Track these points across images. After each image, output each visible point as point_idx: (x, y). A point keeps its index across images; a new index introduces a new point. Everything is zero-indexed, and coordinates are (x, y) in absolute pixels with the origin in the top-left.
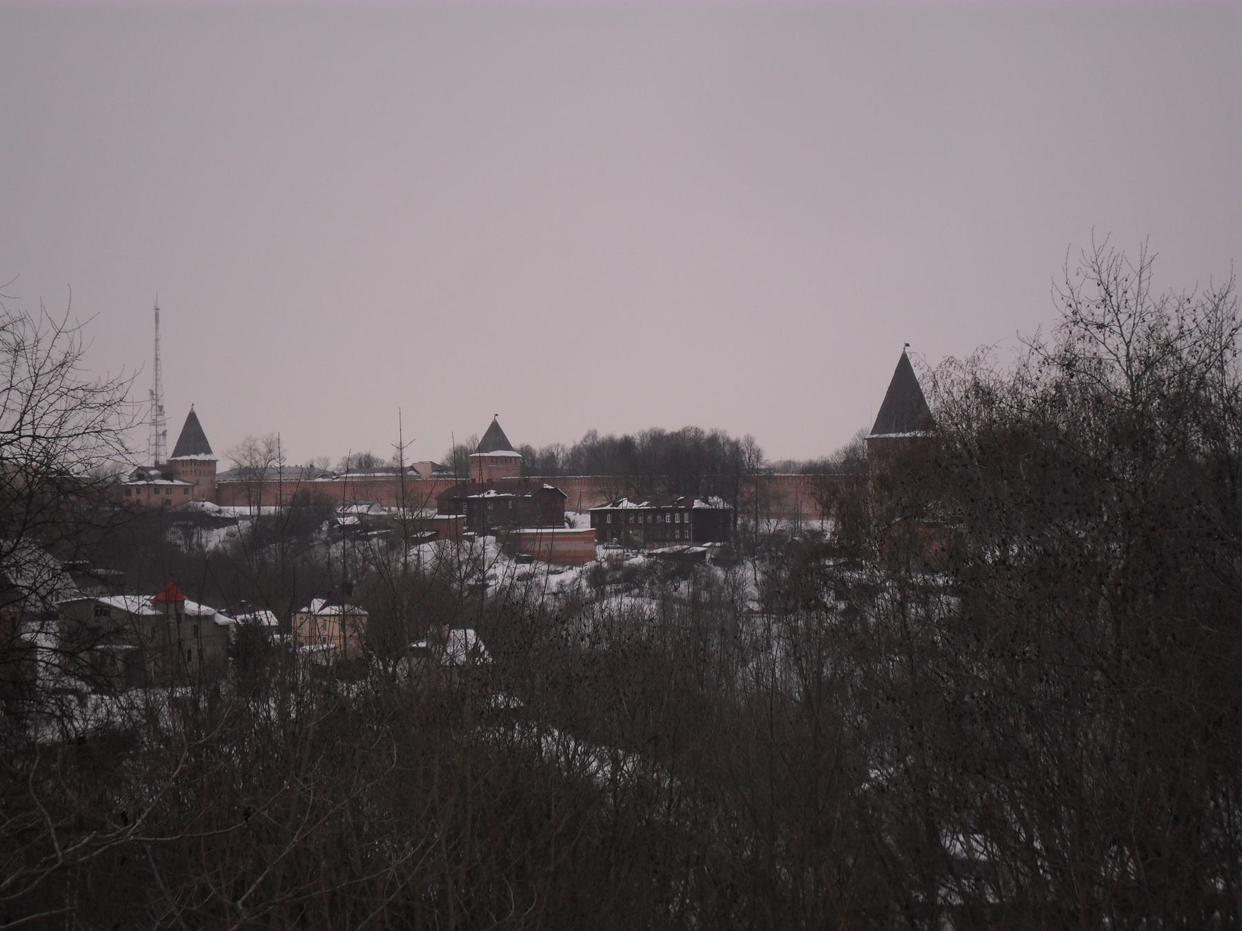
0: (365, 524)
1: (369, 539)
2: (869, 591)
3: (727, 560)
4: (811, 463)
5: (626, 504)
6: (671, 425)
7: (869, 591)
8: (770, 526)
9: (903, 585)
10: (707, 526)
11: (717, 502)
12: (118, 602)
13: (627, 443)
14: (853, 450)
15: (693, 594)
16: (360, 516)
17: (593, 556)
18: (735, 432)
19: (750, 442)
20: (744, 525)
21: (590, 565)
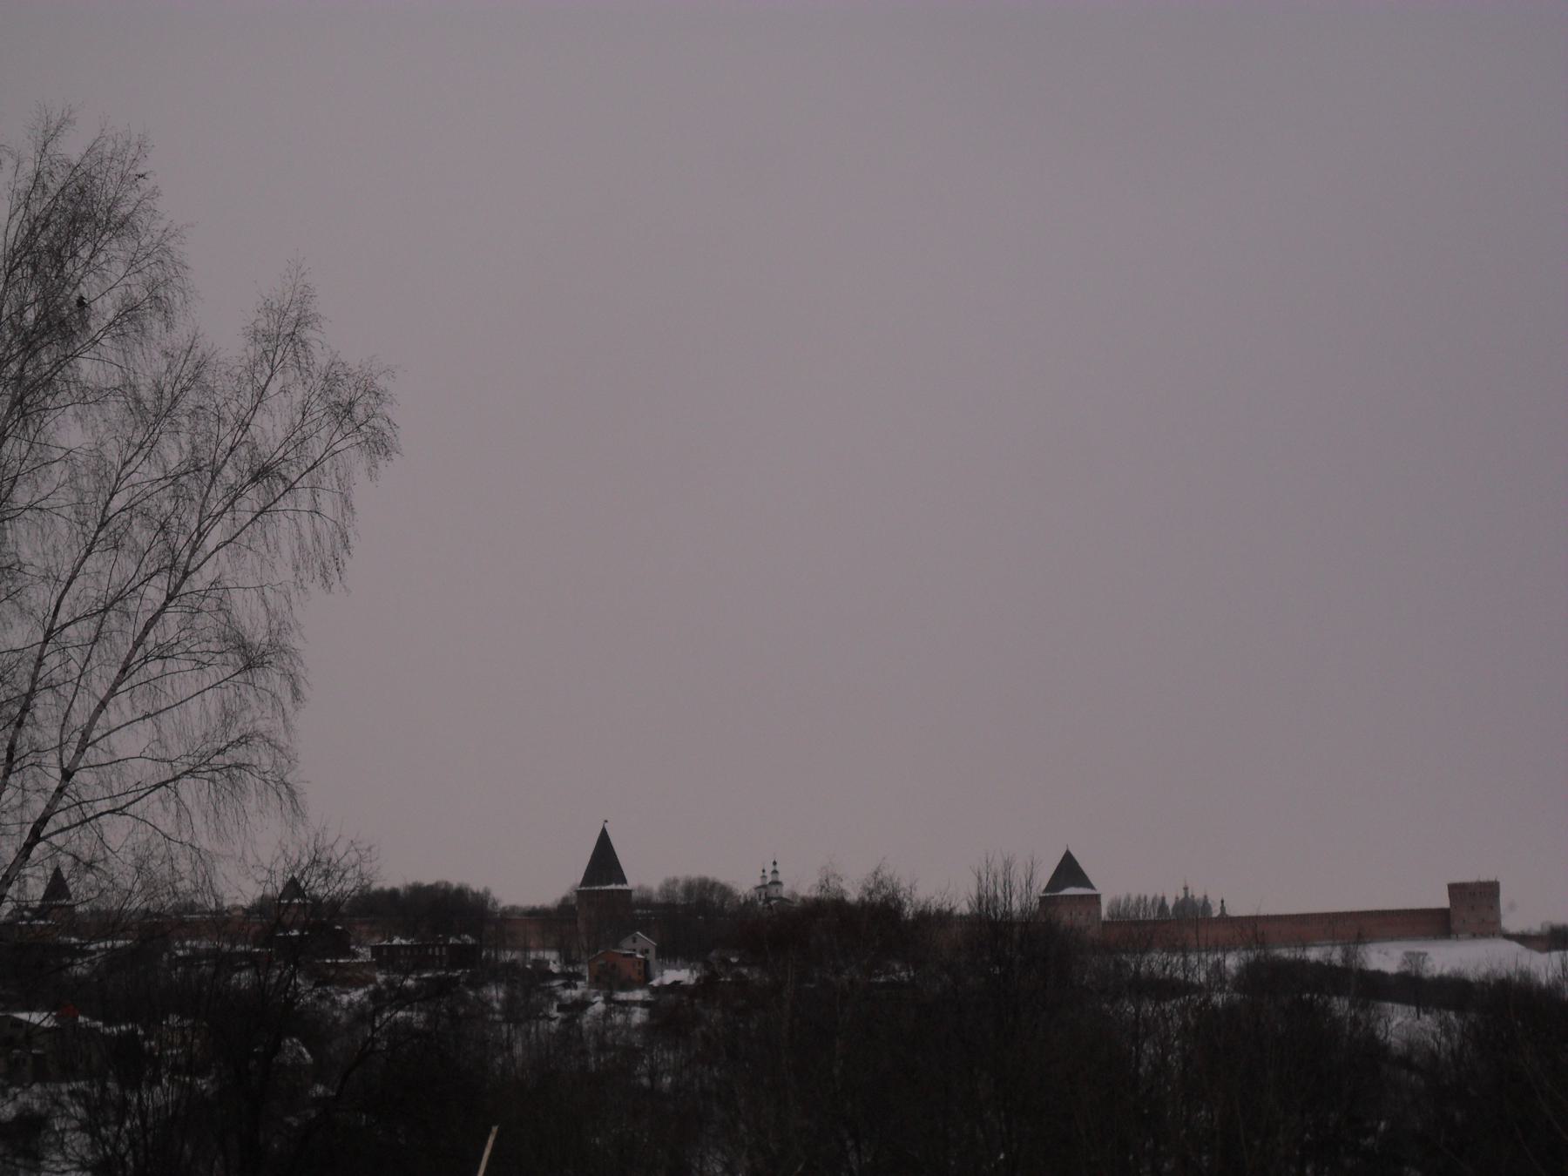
0: (195, 956)
1: (199, 966)
2: (583, 1004)
3: (476, 983)
4: (461, 893)
5: (396, 941)
6: (428, 880)
7: (583, 1004)
8: (508, 956)
9: (608, 1000)
10: (463, 956)
11: (469, 939)
12: (24, 1016)
13: (394, 893)
14: (565, 899)
15: (1441, 1024)
16: (193, 949)
17: (374, 980)
18: (476, 885)
19: (487, 892)
20: (488, 955)
21: (371, 987)
